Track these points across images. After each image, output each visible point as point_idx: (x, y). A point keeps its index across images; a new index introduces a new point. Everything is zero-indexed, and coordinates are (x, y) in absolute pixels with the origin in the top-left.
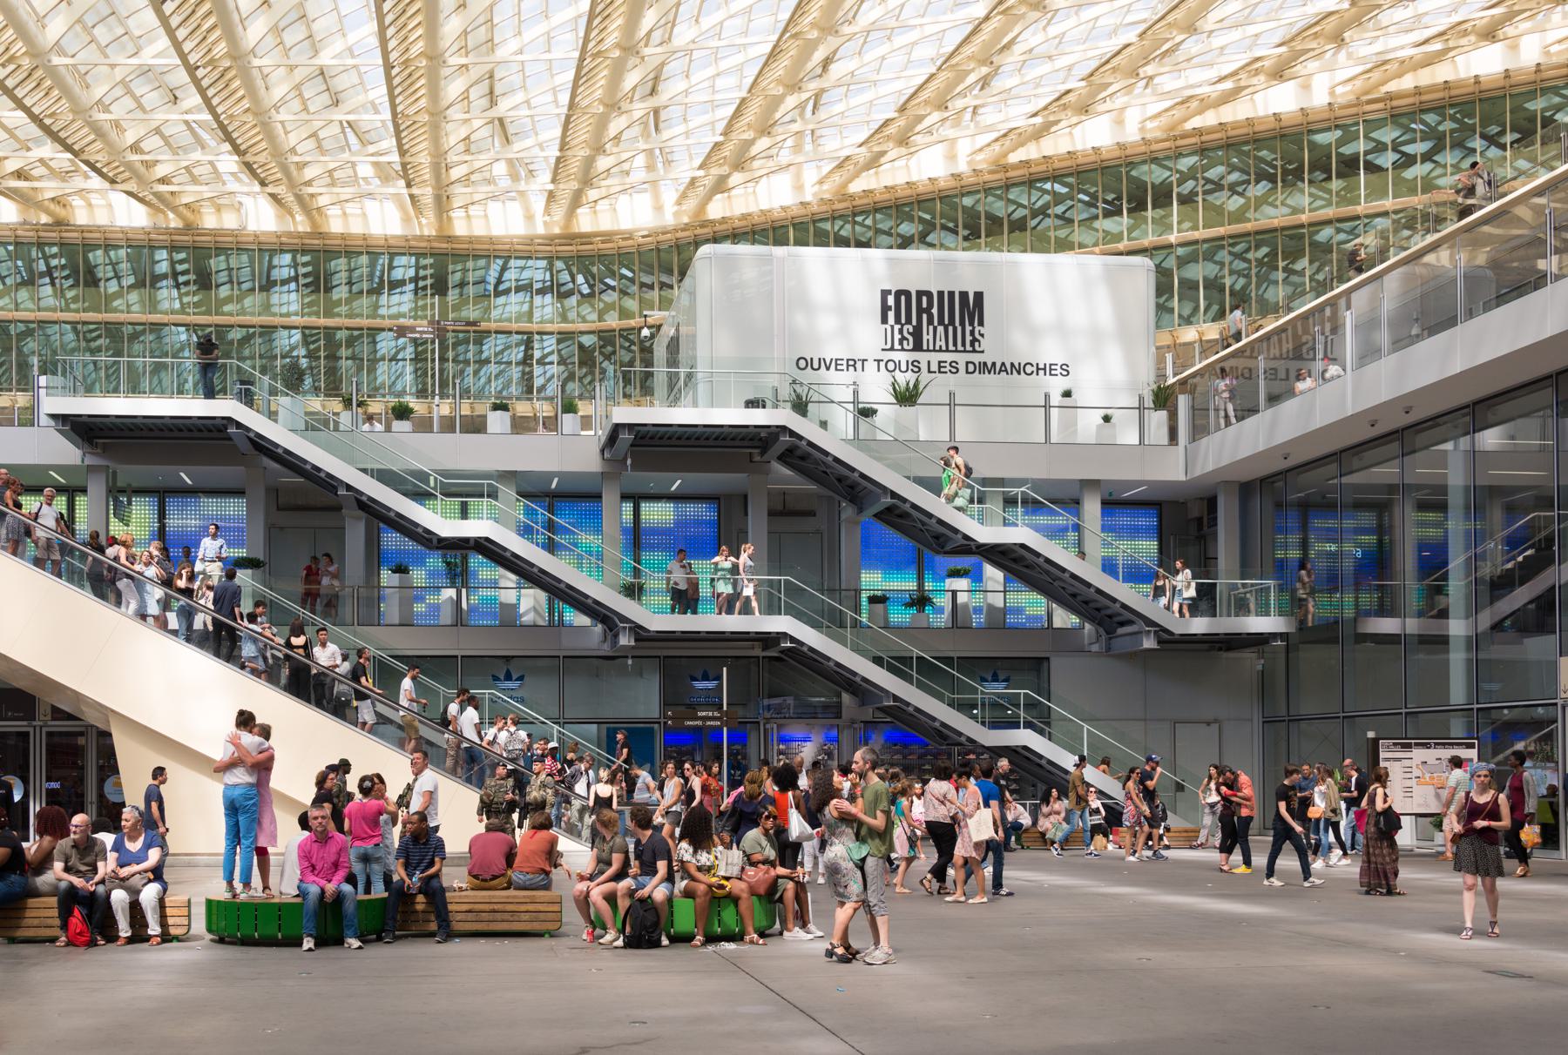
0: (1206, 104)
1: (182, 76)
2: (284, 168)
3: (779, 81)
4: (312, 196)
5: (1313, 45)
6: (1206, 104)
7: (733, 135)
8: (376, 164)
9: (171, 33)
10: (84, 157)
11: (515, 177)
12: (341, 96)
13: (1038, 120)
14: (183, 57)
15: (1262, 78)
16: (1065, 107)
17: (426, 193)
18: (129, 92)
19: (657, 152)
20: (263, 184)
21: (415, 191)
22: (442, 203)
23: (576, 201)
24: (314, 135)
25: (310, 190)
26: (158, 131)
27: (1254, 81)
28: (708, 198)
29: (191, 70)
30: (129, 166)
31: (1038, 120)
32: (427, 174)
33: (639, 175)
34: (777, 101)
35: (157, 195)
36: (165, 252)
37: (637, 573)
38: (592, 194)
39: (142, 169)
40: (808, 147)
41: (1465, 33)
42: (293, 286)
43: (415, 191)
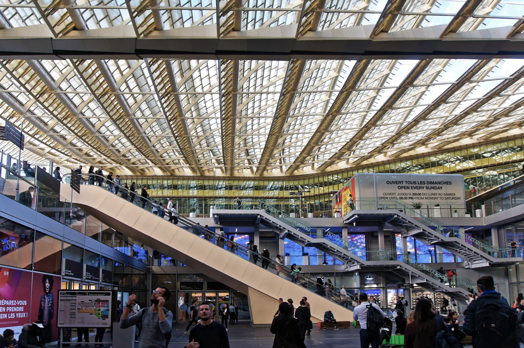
0: (449, 143)
1: (173, 139)
2: (195, 161)
3: (314, 143)
4: (201, 167)
5: (433, 136)
6: (449, 143)
7: (302, 155)
8: (216, 160)
9: (171, 129)
10: (149, 158)
11: (250, 164)
12: (209, 144)
13: (370, 154)
14: (174, 134)
15: (376, 153)
16: (375, 151)
17: (229, 166)
18: (160, 142)
19: (282, 159)
20: (190, 165)
21: (226, 166)
22: (232, 169)
23: (264, 169)
24: (203, 153)
25: (201, 166)
26: (166, 152)
27: (375, 153)
28: (294, 170)
29: (176, 138)
30: (159, 160)
31: (370, 154)
32: (229, 162)
33: (278, 164)
34: (313, 147)
35: (165, 167)
36: (363, 237)
37: (194, 187)
38: (268, 168)
39: (163, 161)
40: (316, 160)
41: (464, 135)
42: (196, 188)
43: (226, 166)
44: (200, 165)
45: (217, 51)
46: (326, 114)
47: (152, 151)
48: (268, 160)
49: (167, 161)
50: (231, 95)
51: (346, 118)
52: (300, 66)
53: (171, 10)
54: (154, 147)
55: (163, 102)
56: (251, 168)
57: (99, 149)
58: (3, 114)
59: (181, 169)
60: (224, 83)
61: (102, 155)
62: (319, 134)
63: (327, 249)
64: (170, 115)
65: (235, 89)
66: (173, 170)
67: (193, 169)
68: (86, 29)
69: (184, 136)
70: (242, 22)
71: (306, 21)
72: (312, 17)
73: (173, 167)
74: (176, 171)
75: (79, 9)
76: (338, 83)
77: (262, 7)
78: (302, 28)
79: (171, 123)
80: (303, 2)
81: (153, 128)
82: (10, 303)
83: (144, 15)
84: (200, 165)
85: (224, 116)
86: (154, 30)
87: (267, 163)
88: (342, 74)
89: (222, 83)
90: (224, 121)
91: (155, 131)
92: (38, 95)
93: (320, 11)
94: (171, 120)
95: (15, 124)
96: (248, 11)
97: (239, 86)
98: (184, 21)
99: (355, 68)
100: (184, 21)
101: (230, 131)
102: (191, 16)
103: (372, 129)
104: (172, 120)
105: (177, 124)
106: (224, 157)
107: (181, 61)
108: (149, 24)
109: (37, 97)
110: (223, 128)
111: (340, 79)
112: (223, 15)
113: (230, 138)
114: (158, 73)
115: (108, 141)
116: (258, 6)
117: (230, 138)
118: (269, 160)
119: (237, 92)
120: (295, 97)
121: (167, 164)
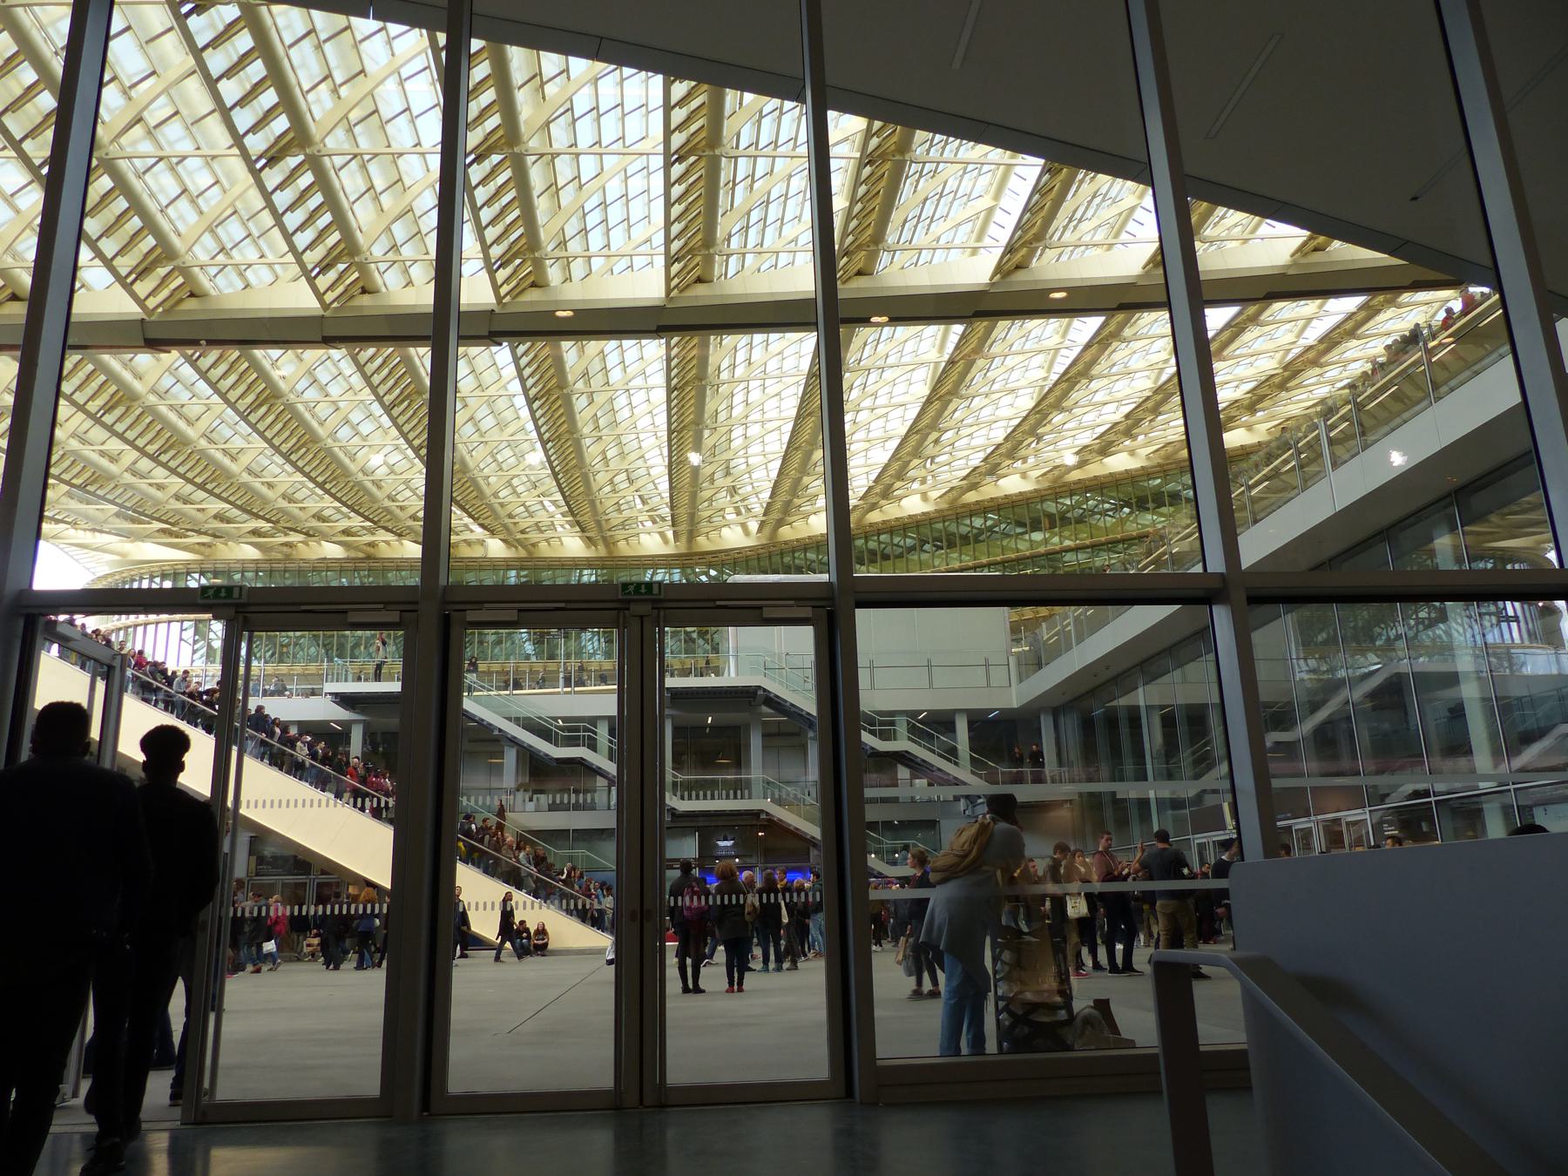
23: (780, 523)
26: (523, 505)
44: (610, 530)
45: (658, 327)
46: (946, 357)
47: (490, 507)
48: (798, 481)
49: (523, 526)
50: (698, 259)
51: (992, 368)
52: (880, 209)
53: (555, 155)
54: (496, 495)
55: (489, 241)
56: (744, 526)
57: (356, 508)
58: (90, 402)
59: (554, 542)
60: (678, 219)
61: (352, 514)
62: (916, 438)
63: (917, 763)
64: (534, 385)
65: (709, 241)
66: (534, 545)
67: (590, 541)
68: (384, 289)
69: (567, 436)
70: (726, 122)
71: (872, 174)
72: (895, 139)
73: (534, 536)
74: (543, 545)
75: (329, 156)
76: (993, 229)
77: (768, 151)
78: (854, 223)
79: (536, 405)
80: (847, 204)
81: (498, 456)
82: (695, 902)
83: (484, 129)
84: (610, 530)
85: (675, 381)
86: (532, 286)
87: (788, 508)
88: (1005, 202)
89: (672, 276)
90: (676, 393)
91: (501, 460)
92: (134, 276)
93: (901, 158)
94: (536, 399)
95: (146, 449)
96: (736, 158)
97: (720, 233)
98: (576, 117)
99: (963, 336)
100: (576, 117)
101: (692, 416)
102: (602, 200)
103: (1025, 443)
104: (539, 399)
105: (541, 377)
106: (672, 508)
107: (584, 343)
108: (513, 238)
109: (129, 280)
110: (673, 412)
111: (998, 216)
112: (680, 160)
113: (691, 433)
114: (499, 228)
115: (379, 487)
116: (761, 145)
117: (691, 433)
118: (800, 479)
119: (717, 249)
120: (907, 178)
121: (523, 532)
